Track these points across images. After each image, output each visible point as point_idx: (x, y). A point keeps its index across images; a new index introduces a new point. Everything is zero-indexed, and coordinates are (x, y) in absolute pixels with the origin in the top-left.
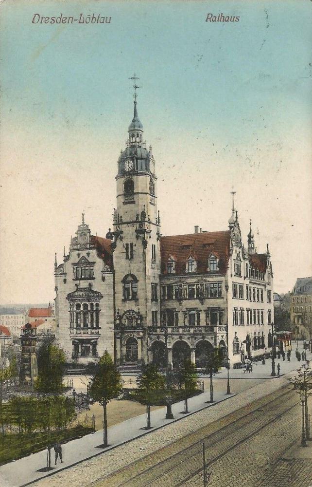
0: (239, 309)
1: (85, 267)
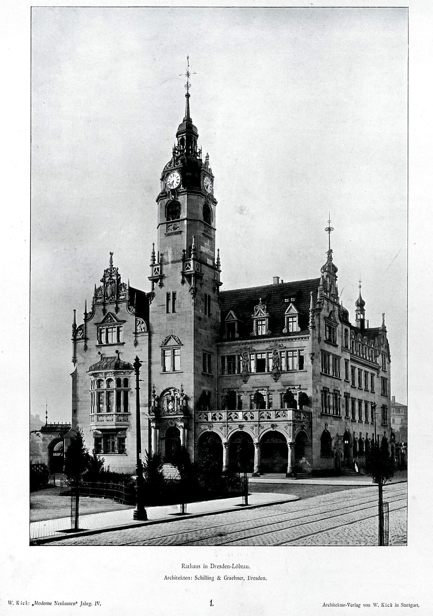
0: (331, 391)
1: (112, 328)
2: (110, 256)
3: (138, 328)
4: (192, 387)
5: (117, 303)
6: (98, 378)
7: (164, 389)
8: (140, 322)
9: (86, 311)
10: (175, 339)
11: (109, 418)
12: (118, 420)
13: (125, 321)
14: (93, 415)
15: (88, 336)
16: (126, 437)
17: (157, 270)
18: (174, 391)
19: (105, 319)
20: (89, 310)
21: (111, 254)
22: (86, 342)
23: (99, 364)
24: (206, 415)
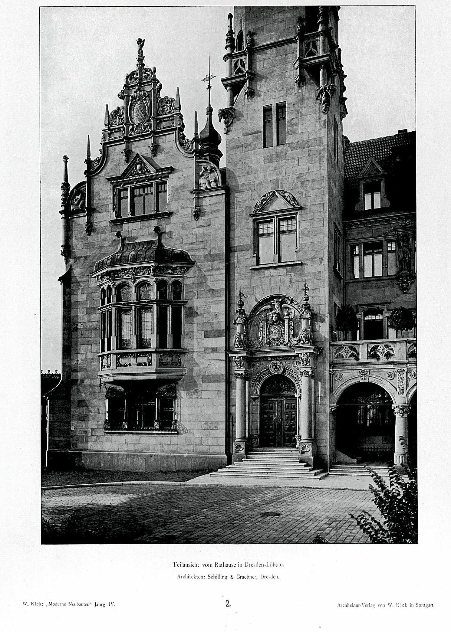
2: (137, 47)
3: (202, 180)
4: (325, 291)
5: (155, 134)
6: (118, 282)
7: (260, 298)
8: (206, 169)
9: (89, 154)
10: (284, 197)
11: (143, 359)
12: (160, 364)
13: (172, 170)
14: (107, 355)
15: (96, 203)
16: (176, 397)
17: (239, 66)
18: (282, 303)
19: (127, 170)
20: (96, 155)
21: (141, 43)
22: (90, 215)
23: (119, 255)
24: (354, 350)
